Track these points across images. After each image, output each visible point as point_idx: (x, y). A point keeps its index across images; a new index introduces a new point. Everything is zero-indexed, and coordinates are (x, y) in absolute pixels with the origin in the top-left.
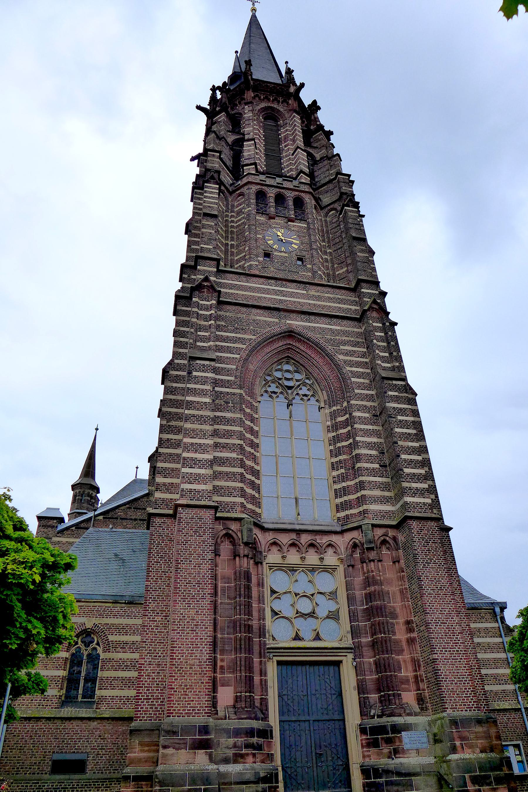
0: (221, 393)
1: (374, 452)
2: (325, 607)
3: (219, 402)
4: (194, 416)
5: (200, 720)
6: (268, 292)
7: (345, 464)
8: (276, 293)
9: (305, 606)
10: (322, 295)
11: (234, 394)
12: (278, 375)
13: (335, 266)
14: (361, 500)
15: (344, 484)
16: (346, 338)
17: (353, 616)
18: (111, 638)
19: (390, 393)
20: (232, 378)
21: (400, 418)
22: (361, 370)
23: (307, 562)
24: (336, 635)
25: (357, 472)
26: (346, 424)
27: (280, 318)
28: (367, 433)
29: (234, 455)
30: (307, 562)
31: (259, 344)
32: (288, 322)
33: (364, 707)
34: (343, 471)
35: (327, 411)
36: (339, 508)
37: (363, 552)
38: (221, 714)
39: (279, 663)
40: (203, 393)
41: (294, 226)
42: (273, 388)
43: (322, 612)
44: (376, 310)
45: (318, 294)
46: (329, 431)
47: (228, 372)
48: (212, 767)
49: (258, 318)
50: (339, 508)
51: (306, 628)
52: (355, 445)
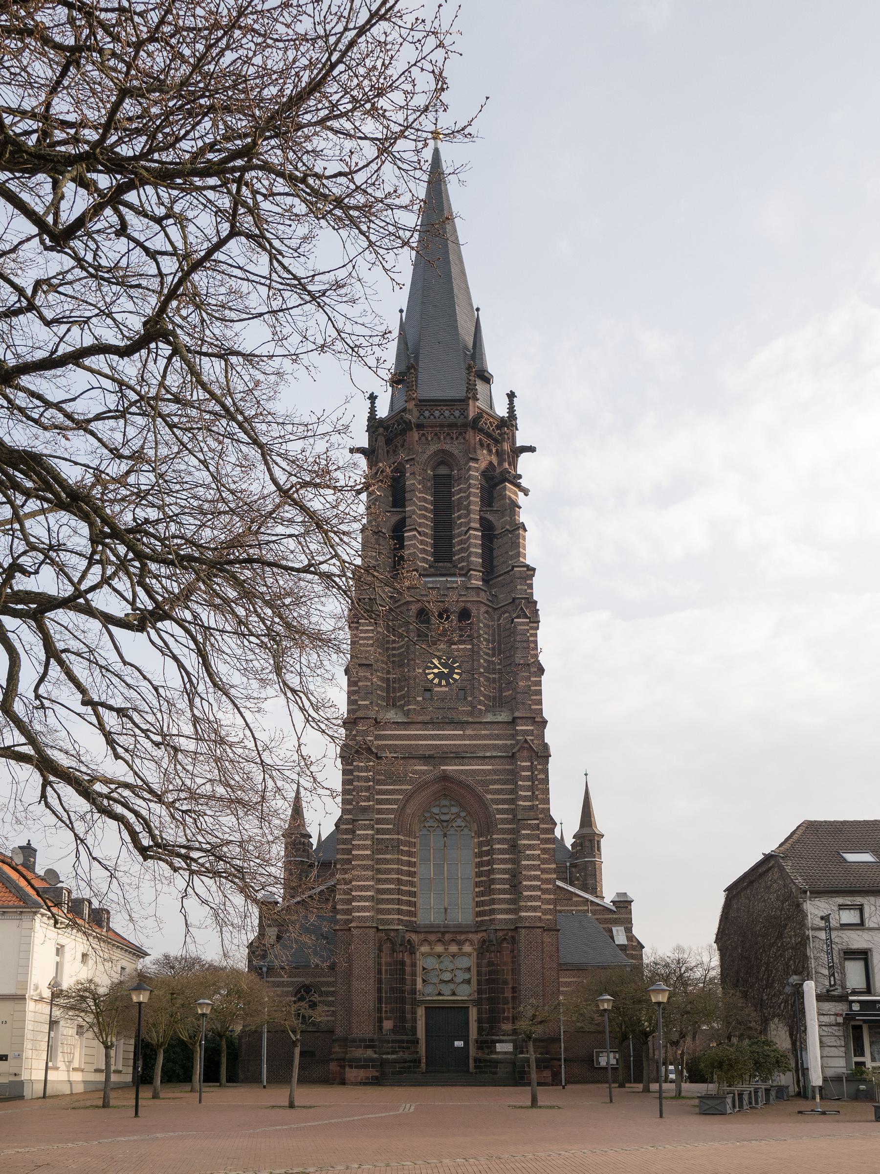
1: (507, 876)
2: (461, 976)
3: (380, 847)
4: (359, 865)
6: (425, 737)
7: (485, 885)
8: (433, 738)
9: (447, 976)
10: (479, 732)
11: (393, 839)
12: (436, 810)
13: (504, 685)
15: (482, 899)
16: (496, 777)
17: (479, 982)
18: (323, 989)
19: (523, 832)
21: (528, 852)
23: (450, 951)
24: (465, 993)
25: (491, 892)
26: (488, 853)
27: (434, 766)
28: (503, 861)
29: (393, 886)
30: (450, 951)
31: (415, 792)
32: (442, 768)
33: (480, 1030)
34: (482, 889)
36: (479, 914)
37: (484, 948)
38: (384, 1033)
39: (426, 1007)
40: (364, 847)
42: (431, 823)
43: (458, 979)
44: (527, 749)
45: (475, 732)
46: (476, 857)
47: (387, 821)
48: (375, 1056)
50: (479, 914)
51: (446, 989)
52: (492, 871)
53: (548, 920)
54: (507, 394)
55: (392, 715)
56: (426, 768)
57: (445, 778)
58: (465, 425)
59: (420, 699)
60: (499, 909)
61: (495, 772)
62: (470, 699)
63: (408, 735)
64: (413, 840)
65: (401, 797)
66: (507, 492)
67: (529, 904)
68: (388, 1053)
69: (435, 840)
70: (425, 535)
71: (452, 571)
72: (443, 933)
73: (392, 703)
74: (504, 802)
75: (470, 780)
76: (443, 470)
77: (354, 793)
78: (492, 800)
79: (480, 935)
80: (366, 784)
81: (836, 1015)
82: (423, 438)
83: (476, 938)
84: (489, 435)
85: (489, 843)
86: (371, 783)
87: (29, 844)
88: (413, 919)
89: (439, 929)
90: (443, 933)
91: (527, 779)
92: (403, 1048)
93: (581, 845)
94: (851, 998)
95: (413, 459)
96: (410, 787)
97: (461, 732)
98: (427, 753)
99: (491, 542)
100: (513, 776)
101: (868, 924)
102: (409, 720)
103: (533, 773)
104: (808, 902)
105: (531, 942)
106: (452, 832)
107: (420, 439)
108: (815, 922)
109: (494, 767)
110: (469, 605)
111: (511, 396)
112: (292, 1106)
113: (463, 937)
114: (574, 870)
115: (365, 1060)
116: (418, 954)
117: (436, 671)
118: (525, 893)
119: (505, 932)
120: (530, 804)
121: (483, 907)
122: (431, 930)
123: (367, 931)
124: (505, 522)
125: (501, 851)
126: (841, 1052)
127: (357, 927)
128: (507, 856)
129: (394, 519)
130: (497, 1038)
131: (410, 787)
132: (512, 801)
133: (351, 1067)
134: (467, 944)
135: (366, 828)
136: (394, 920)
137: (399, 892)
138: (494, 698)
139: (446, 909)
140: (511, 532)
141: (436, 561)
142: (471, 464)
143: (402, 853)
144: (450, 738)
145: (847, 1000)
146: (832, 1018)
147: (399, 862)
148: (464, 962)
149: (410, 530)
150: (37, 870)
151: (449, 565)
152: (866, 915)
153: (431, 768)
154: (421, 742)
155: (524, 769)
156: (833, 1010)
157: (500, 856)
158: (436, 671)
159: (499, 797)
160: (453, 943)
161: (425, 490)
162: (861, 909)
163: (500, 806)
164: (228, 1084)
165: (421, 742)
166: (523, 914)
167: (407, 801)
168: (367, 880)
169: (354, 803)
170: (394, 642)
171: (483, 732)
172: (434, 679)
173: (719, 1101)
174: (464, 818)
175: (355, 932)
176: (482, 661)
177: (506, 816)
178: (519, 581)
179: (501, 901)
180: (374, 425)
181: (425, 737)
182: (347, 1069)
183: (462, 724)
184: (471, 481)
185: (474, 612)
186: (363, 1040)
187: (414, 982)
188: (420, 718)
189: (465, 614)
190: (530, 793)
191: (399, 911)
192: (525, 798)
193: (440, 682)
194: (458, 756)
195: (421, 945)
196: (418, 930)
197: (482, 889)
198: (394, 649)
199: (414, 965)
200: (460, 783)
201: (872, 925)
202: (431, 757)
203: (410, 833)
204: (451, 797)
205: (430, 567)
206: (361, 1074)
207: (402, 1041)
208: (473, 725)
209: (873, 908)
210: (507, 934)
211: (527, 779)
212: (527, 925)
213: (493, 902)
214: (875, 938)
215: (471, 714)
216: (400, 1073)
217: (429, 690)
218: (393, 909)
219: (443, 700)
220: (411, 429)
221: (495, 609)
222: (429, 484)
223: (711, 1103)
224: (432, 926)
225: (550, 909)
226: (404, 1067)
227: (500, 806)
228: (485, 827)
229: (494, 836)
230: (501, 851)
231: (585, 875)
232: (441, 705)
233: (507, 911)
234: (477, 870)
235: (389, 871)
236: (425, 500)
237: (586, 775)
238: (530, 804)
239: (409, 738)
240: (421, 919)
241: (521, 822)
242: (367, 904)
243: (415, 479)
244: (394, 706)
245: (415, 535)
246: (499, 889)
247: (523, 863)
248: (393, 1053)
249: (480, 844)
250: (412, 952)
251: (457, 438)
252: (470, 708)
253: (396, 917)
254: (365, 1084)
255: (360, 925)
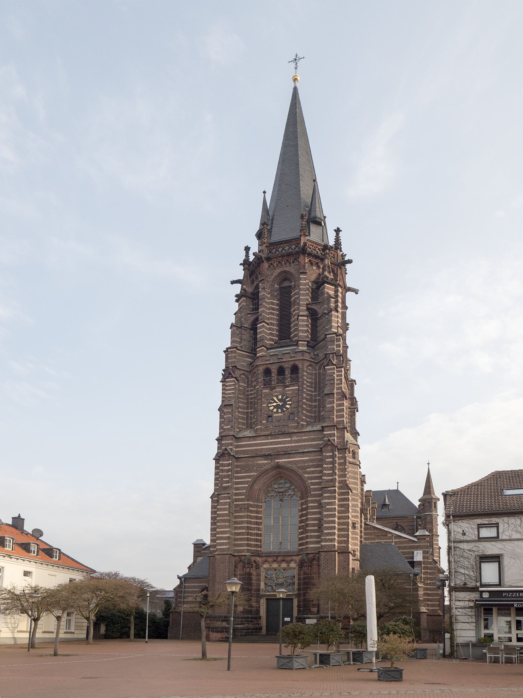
0: (238, 504)
1: (316, 522)
5: (225, 614)
6: (267, 444)
7: (303, 528)
8: (271, 444)
10: (301, 438)
11: (245, 504)
12: (276, 486)
14: (307, 543)
17: (299, 584)
20: (244, 497)
21: (327, 507)
22: (318, 481)
27: (271, 460)
28: (314, 513)
29: (244, 531)
31: (259, 476)
32: (276, 461)
33: (299, 611)
34: (302, 530)
35: (300, 502)
36: (300, 545)
37: (301, 565)
40: (224, 509)
41: (289, 390)
45: (298, 438)
46: (300, 512)
47: (241, 494)
49: (259, 462)
50: (300, 545)
52: (307, 520)
53: (343, 547)
54: (335, 230)
55: (248, 433)
56: (266, 462)
57: (278, 466)
58: (298, 253)
59: (265, 422)
60: (311, 541)
61: (311, 461)
62: (296, 419)
63: (255, 444)
64: (260, 504)
65: (250, 480)
66: (326, 290)
67: (328, 537)
68: (238, 624)
69: (275, 503)
70: (272, 324)
71: (292, 343)
72: (277, 556)
73: (249, 426)
74: (316, 478)
75: (294, 467)
76: (286, 284)
77: (220, 479)
78: (308, 477)
79: (300, 557)
80: (227, 474)
81: (469, 601)
82: (272, 266)
83: (298, 558)
84: (316, 257)
85: (306, 503)
86: (230, 473)
87: (19, 516)
88: (259, 549)
89: (275, 555)
90: (277, 556)
91: (330, 463)
92: (248, 621)
93: (423, 505)
94: (480, 589)
95: (263, 279)
96: (256, 474)
97: (290, 439)
98: (267, 453)
99: (316, 322)
100: (320, 463)
101: (502, 536)
102: (257, 435)
103: (334, 459)
104: (452, 523)
105: (328, 560)
106: (286, 498)
107: (269, 267)
108: (457, 537)
109: (310, 458)
110: (297, 362)
111: (338, 231)
112: (55, 654)
113: (289, 558)
114: (419, 520)
115: (221, 628)
116: (262, 569)
117: (275, 404)
118: (325, 531)
119: (314, 555)
120: (331, 478)
121: (302, 541)
122: (269, 555)
123: (225, 556)
124: (324, 309)
125: (313, 508)
126: (472, 626)
127: (219, 554)
128: (317, 510)
129: (252, 318)
130: (307, 616)
131: (256, 474)
132: (320, 478)
133: (213, 632)
134: (293, 562)
135: (225, 498)
136: (244, 550)
137: (248, 534)
138: (315, 417)
139: (281, 543)
140: (327, 314)
141: (280, 339)
142: (301, 276)
143: (251, 511)
144: (283, 443)
145: (478, 591)
146: (467, 603)
147: (248, 516)
148: (289, 573)
149: (260, 323)
150: (25, 528)
151: (289, 340)
152: (501, 530)
153: (270, 461)
154: (263, 447)
155: (328, 457)
156: (468, 597)
157: (312, 511)
158: (275, 404)
159: (312, 475)
160: (284, 562)
161: (273, 297)
162: (497, 525)
163: (313, 481)
164: (136, 640)
165: (263, 447)
166: (323, 544)
167: (254, 482)
168: (226, 527)
169: (219, 485)
170: (251, 390)
171: (304, 438)
172: (273, 409)
173: (289, 660)
174: (293, 489)
175: (217, 557)
176: (305, 395)
177: (317, 486)
178: (329, 343)
179: (312, 537)
180: (246, 263)
181: (267, 444)
182: (211, 633)
183: (290, 434)
184: (301, 287)
185: (300, 366)
186: (219, 617)
187: (259, 585)
188: (264, 433)
189: (295, 369)
190: (331, 472)
191: (248, 545)
192: (329, 475)
193: (277, 411)
194: (287, 453)
195: (264, 564)
196: (261, 555)
197: (302, 530)
198: (251, 394)
199: (259, 575)
200: (287, 469)
201: (504, 537)
202: (269, 455)
203: (258, 500)
204: (282, 478)
205: (275, 343)
206: (219, 635)
207: (248, 618)
208: (297, 434)
209: (506, 525)
210: (315, 556)
211: (330, 463)
212: (325, 550)
213: (307, 537)
214: (506, 547)
215: (297, 427)
216: (245, 635)
217: (271, 416)
218: (244, 544)
219: (279, 421)
220: (263, 262)
221: (317, 363)
222: (276, 293)
223: (285, 661)
224: (271, 553)
225: (344, 540)
226: (248, 632)
227: (313, 481)
228: (304, 493)
229: (309, 499)
230: (313, 508)
231: (426, 523)
232: (278, 424)
233: (316, 543)
234: (300, 519)
235: (242, 522)
236: (272, 303)
237: (428, 464)
238: (331, 478)
239: (256, 445)
240: (264, 549)
241: (324, 489)
242: (225, 541)
243: (265, 291)
244: (251, 427)
245: (263, 325)
246: (311, 530)
247: (324, 513)
248: (241, 624)
249: (302, 504)
250: (258, 567)
251: (293, 262)
252: (296, 424)
253: (246, 548)
254: (221, 641)
255: (220, 553)
